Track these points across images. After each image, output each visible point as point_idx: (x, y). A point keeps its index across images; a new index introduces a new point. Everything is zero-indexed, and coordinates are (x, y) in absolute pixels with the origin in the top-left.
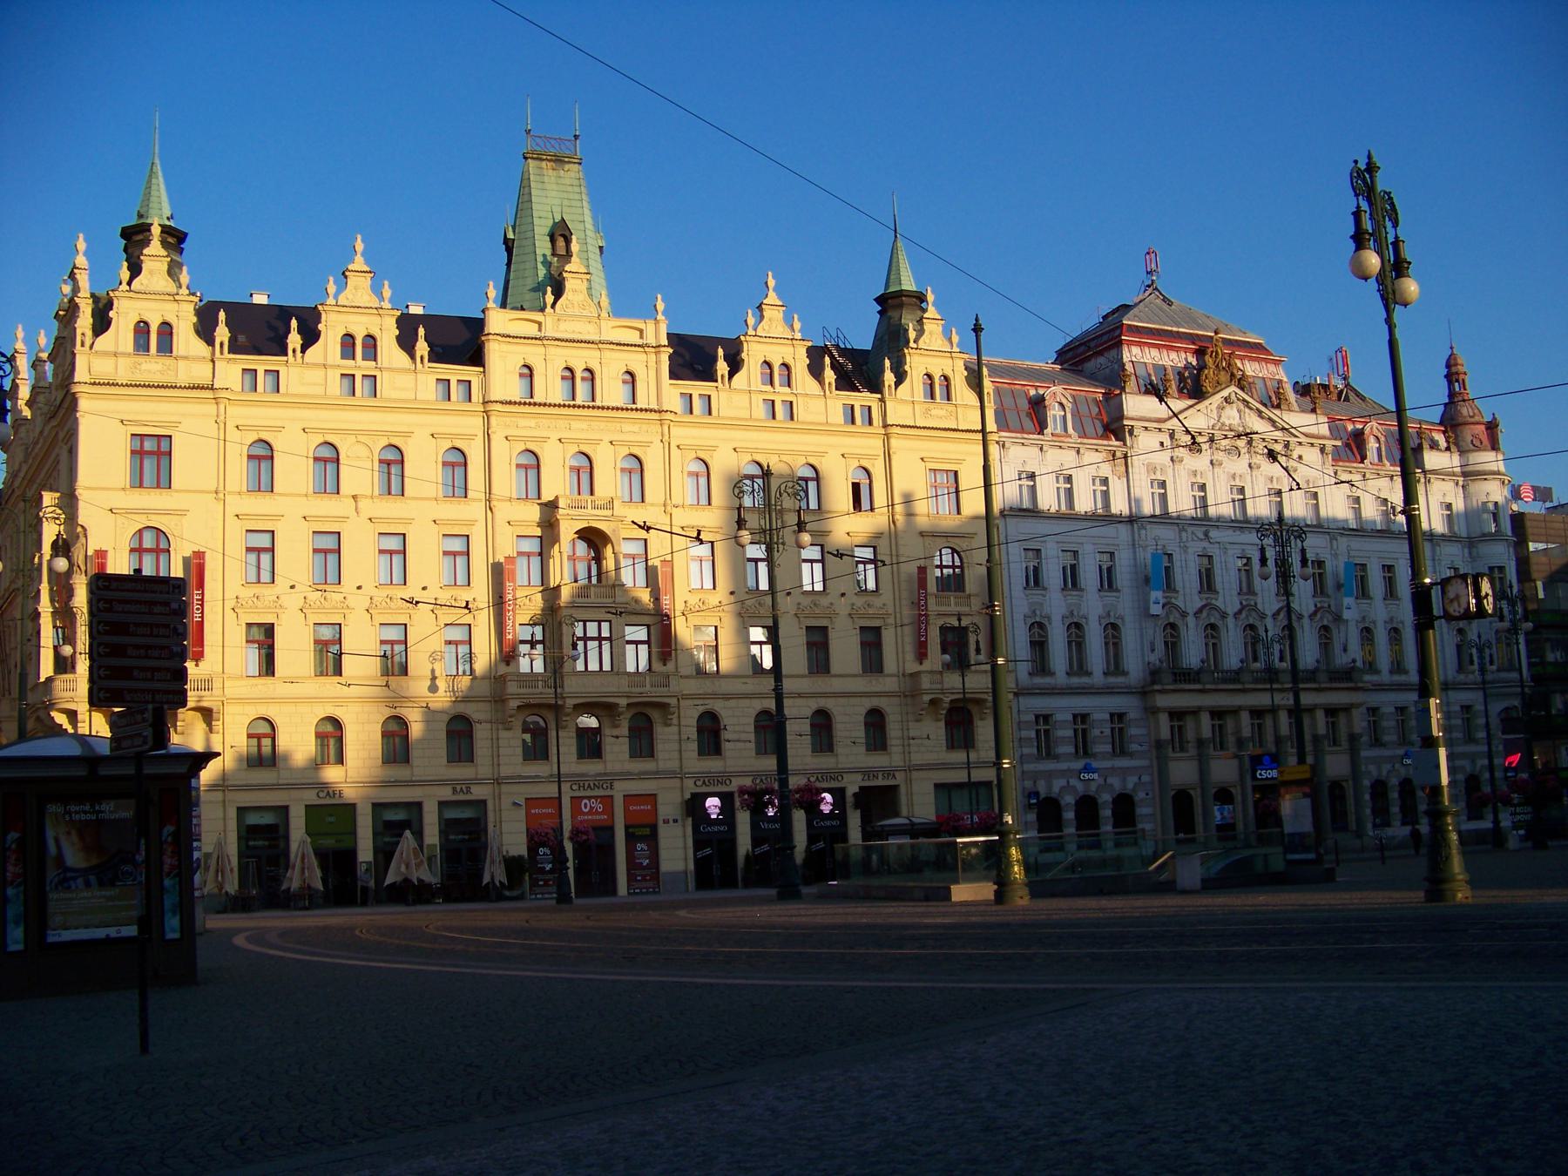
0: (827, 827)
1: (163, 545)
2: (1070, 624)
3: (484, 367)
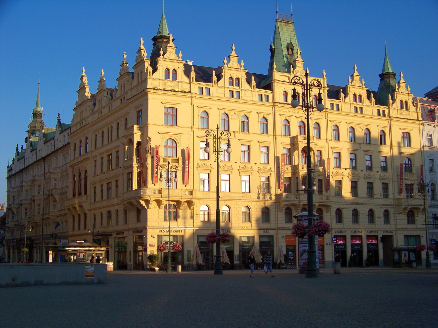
0: (373, 248)
3: (272, 90)
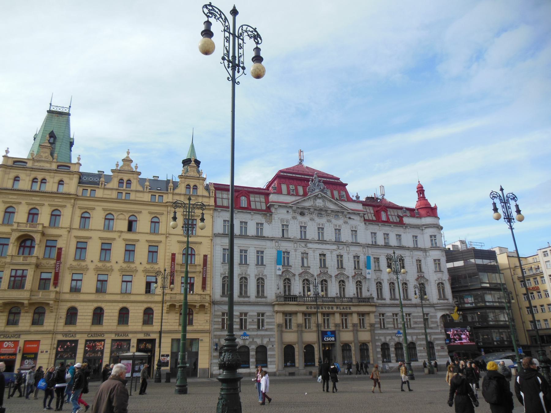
1: (193, 253)
2: (403, 283)
